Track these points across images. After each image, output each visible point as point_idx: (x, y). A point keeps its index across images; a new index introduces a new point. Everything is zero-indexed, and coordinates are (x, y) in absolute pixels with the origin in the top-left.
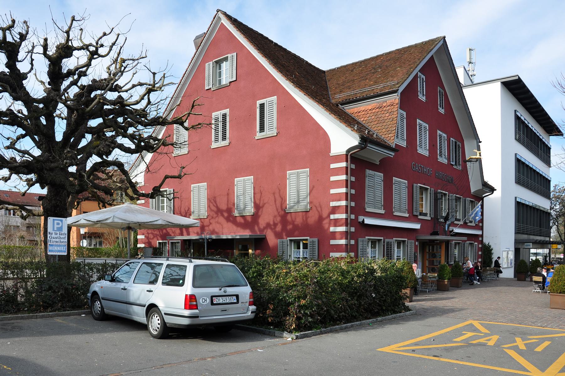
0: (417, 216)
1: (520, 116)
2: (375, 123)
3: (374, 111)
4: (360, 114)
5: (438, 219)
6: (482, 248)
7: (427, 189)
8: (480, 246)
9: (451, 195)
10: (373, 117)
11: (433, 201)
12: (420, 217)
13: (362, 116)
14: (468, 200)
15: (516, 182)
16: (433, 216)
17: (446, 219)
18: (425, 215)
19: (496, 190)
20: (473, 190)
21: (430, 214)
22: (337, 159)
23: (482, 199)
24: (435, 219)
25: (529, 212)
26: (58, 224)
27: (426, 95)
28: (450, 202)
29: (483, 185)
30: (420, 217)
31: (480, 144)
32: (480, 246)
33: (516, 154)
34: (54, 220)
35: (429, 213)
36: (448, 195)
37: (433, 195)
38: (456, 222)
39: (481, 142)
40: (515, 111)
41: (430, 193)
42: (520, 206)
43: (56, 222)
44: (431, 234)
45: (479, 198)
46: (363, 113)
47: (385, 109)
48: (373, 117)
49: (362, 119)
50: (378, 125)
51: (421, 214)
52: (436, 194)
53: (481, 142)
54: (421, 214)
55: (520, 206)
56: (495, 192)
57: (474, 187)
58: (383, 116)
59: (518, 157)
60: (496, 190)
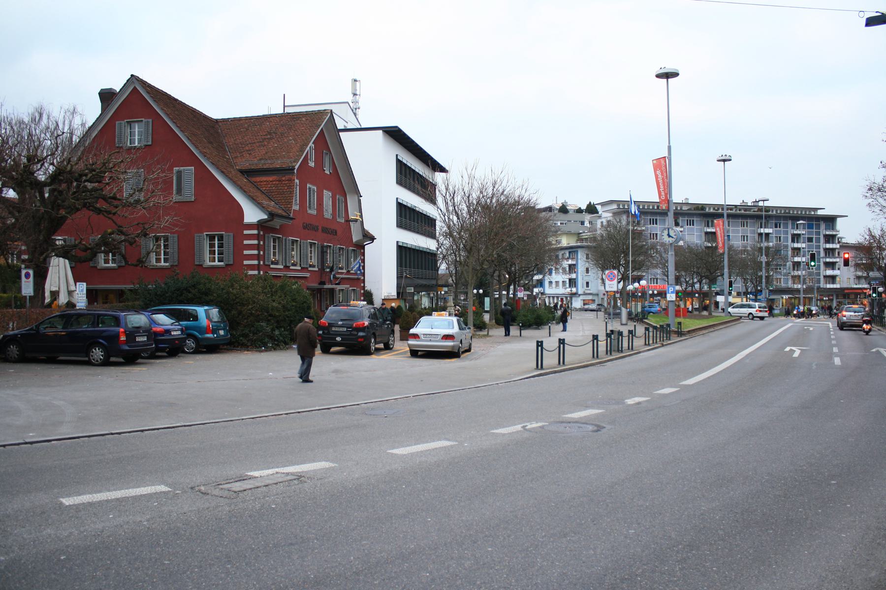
0: (307, 268)
1: (401, 159)
2: (276, 193)
3: (274, 182)
4: (262, 183)
5: (324, 269)
6: (364, 293)
7: (315, 243)
8: (362, 291)
9: (302, 241)
10: (274, 188)
11: (320, 254)
12: (310, 269)
13: (263, 186)
14: (289, 240)
15: (397, 183)
16: (320, 267)
17: (332, 269)
18: (314, 266)
19: (376, 239)
20: (355, 239)
21: (318, 266)
22: (250, 226)
23: (363, 247)
24: (322, 269)
25: (424, 256)
26: (81, 287)
27: (315, 161)
28: (334, 254)
29: (363, 236)
30: (310, 269)
31: (361, 198)
32: (362, 291)
33: (397, 199)
34: (80, 284)
35: (316, 264)
36: (299, 241)
37: (320, 249)
38: (340, 271)
39: (361, 196)
40: (397, 155)
41: (318, 247)
42: (403, 251)
43: (81, 285)
44: (320, 284)
45: (360, 248)
46: (265, 183)
47: (284, 182)
48: (274, 188)
49: (264, 189)
50: (278, 196)
51: (311, 266)
52: (323, 247)
53: (361, 196)
54: (311, 266)
55: (403, 251)
56: (375, 240)
57: (356, 237)
58: (282, 188)
59: (399, 201)
60: (376, 239)
